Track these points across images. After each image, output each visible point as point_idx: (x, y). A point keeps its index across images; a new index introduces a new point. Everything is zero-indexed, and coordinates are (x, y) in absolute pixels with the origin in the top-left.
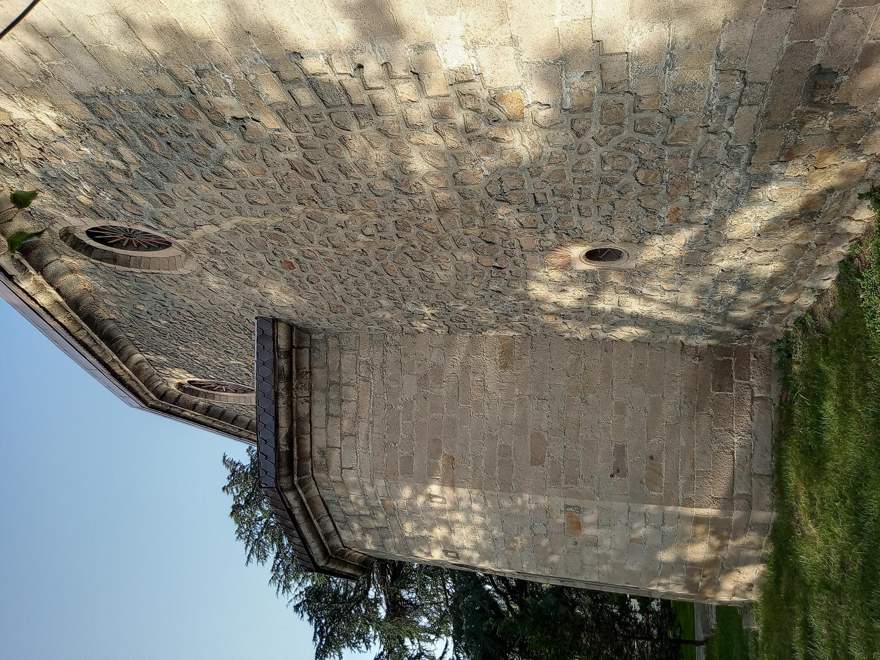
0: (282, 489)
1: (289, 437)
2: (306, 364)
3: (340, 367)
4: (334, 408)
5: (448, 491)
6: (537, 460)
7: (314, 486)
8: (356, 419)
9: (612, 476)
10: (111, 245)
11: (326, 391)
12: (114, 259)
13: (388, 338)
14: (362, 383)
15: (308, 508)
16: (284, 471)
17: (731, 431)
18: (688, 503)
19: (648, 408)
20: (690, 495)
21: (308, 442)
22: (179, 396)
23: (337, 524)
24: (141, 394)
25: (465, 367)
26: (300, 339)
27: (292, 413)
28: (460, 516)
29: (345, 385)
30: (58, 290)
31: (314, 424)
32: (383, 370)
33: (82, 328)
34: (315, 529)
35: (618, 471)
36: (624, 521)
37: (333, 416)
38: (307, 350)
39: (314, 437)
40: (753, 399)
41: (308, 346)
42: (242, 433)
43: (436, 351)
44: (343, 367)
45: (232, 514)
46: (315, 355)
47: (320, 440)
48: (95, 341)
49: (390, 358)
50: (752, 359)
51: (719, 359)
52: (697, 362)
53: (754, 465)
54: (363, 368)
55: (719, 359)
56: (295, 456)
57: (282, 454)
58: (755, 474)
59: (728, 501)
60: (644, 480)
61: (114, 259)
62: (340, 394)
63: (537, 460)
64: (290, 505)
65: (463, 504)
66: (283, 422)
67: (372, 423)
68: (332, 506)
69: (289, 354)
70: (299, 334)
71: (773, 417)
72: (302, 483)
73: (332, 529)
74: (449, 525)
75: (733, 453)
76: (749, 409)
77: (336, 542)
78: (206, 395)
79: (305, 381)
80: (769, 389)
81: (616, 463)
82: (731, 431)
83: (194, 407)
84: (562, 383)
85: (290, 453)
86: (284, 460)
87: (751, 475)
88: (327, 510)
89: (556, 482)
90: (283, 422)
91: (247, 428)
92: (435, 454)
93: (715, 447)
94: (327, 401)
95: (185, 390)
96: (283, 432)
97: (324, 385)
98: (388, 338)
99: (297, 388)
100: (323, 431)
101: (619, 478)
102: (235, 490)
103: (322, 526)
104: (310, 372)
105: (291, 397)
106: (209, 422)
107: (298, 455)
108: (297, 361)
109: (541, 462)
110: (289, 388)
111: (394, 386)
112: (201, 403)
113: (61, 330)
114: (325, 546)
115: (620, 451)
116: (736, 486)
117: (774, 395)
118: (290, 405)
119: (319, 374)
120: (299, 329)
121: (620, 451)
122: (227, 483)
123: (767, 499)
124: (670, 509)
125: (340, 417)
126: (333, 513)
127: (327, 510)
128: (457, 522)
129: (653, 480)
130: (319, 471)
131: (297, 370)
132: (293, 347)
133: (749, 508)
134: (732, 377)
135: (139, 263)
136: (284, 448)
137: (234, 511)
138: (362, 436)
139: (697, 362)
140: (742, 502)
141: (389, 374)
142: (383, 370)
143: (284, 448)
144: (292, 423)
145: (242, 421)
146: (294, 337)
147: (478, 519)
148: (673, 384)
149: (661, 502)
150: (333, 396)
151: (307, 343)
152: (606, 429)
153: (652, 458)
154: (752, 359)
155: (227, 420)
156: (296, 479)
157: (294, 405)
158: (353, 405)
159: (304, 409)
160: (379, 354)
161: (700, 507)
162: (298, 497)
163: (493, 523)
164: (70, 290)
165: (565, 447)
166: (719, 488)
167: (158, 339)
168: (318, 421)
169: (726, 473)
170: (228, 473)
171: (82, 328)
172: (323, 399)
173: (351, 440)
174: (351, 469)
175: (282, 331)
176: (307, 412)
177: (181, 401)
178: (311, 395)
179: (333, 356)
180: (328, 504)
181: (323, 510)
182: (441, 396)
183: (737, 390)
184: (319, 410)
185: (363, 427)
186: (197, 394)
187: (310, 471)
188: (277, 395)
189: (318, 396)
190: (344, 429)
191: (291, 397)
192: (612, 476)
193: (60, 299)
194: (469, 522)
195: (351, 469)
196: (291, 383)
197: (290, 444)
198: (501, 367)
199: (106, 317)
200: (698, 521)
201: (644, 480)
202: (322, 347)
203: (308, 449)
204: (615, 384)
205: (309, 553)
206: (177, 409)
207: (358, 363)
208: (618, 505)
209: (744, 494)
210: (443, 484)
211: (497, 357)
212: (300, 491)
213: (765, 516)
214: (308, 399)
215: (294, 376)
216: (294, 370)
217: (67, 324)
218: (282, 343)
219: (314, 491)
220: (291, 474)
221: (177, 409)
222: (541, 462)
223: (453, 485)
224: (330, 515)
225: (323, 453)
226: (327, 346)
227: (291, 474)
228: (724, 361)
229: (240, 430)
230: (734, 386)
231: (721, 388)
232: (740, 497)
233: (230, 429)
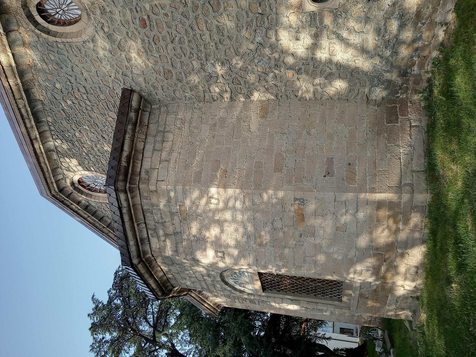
0: (118, 189)
1: (129, 158)
2: (146, 121)
3: (165, 122)
4: (158, 146)
5: (221, 190)
6: (278, 169)
7: (138, 195)
8: (171, 152)
9: (325, 176)
10: (49, 22)
11: (155, 136)
12: (48, 32)
13: (196, 105)
14: (177, 130)
15: (133, 212)
16: (121, 177)
17: (398, 146)
18: (373, 190)
19: (347, 136)
20: (374, 186)
21: (139, 165)
22: (72, 193)
23: (150, 232)
24: (48, 180)
25: (239, 119)
26: (145, 106)
27: (133, 145)
28: (228, 215)
29: (167, 132)
30: (13, 55)
31: (145, 155)
32: (190, 123)
33: (22, 98)
34: (134, 228)
35: (329, 173)
36: (332, 209)
37: (157, 150)
38: (148, 113)
39: (143, 163)
40: (411, 127)
41: (149, 111)
42: (104, 230)
43: (223, 110)
44: (167, 122)
45: (90, 329)
46: (152, 117)
47: (147, 165)
48: (28, 114)
49: (196, 116)
50: (409, 104)
51: (390, 106)
52: (376, 108)
53: (414, 165)
54: (178, 122)
55: (390, 106)
56: (130, 171)
57: (122, 167)
58: (415, 171)
59: (399, 189)
60: (345, 178)
61: (48, 32)
62: (164, 137)
63: (278, 169)
64: (121, 205)
65: (231, 204)
66: (126, 148)
67: (180, 153)
68: (148, 215)
69: (137, 111)
70: (145, 102)
71: (424, 136)
72: (131, 191)
73: (145, 236)
74: (220, 223)
75: (400, 159)
76: (409, 132)
77: (147, 248)
78: (87, 195)
79: (144, 130)
80: (421, 121)
81: (327, 168)
82: (398, 146)
83: (79, 203)
84: (296, 124)
85: (127, 168)
86: (122, 170)
87: (413, 171)
88: (145, 219)
89: (290, 182)
90: (132, 243)
91: (108, 227)
92: (216, 169)
93: (389, 155)
94: (155, 142)
95: (76, 188)
96: (125, 154)
97: (154, 133)
98: (196, 105)
99: (138, 132)
100: (149, 159)
101: (329, 178)
102: (95, 318)
103: (140, 231)
104: (148, 126)
105: (133, 136)
106: (86, 216)
107: (132, 171)
108: (141, 117)
109: (281, 170)
110: (134, 130)
111: (196, 131)
112: (83, 202)
113: (11, 95)
114: (139, 249)
115: (330, 161)
116: (403, 179)
117: (424, 124)
118: (132, 141)
119: (153, 127)
120: (146, 100)
121: (330, 161)
122: (92, 312)
123: (423, 185)
124: (362, 196)
125: (161, 150)
126: (148, 222)
127: (145, 219)
128: (226, 221)
129: (351, 178)
130: (143, 184)
131: (140, 122)
132: (140, 109)
133: (412, 192)
134: (397, 114)
135: (61, 35)
136: (124, 164)
137: (92, 327)
138: (172, 161)
139: (376, 108)
140: (407, 188)
141: (194, 125)
142: (190, 123)
143: (124, 164)
144: (132, 151)
145: (106, 221)
146: (142, 103)
147: (239, 217)
148: (362, 121)
149: (354, 190)
150: (159, 138)
151: (149, 110)
152: (321, 149)
153: (350, 164)
154: (409, 104)
155: (97, 217)
156: (128, 185)
157: (135, 142)
158: (170, 143)
159: (140, 146)
160: (189, 114)
161: (381, 192)
162: (127, 200)
163: (248, 220)
164: (21, 61)
165: (296, 161)
166: (394, 180)
167: (64, 122)
168: (147, 154)
169: (397, 171)
170: (94, 306)
171: (22, 98)
172: (153, 141)
173: (166, 163)
174: (163, 181)
175: (135, 98)
176: (142, 148)
177: (71, 196)
178: (146, 139)
179: (163, 117)
180: (145, 213)
181: (142, 217)
182: (223, 135)
183: (401, 122)
184: (149, 147)
185: (175, 155)
186: (82, 193)
187: (137, 183)
188: (125, 132)
189: (150, 139)
190: (163, 158)
191: (133, 136)
192: (325, 176)
193: (14, 65)
194: (234, 220)
195: (163, 181)
196: (135, 129)
197: (128, 162)
198: (260, 117)
199: (38, 97)
200: (380, 205)
201: (345, 178)
202: (157, 112)
203: (139, 170)
204: (327, 123)
205: (128, 249)
206: (69, 202)
207: (176, 119)
208: (329, 196)
209: (408, 183)
210: (218, 187)
211: (258, 112)
212: (129, 195)
213: (423, 197)
214: (144, 140)
215: (138, 125)
216: (138, 122)
217: (14, 88)
218: (134, 103)
219: (138, 199)
220: (125, 181)
221: (69, 202)
222: (281, 170)
223: (225, 187)
224: (145, 223)
225: (147, 172)
226: (160, 111)
227: (125, 181)
228: (392, 107)
229: (104, 227)
230: (399, 120)
231: (390, 121)
232: (406, 185)
233: (97, 225)
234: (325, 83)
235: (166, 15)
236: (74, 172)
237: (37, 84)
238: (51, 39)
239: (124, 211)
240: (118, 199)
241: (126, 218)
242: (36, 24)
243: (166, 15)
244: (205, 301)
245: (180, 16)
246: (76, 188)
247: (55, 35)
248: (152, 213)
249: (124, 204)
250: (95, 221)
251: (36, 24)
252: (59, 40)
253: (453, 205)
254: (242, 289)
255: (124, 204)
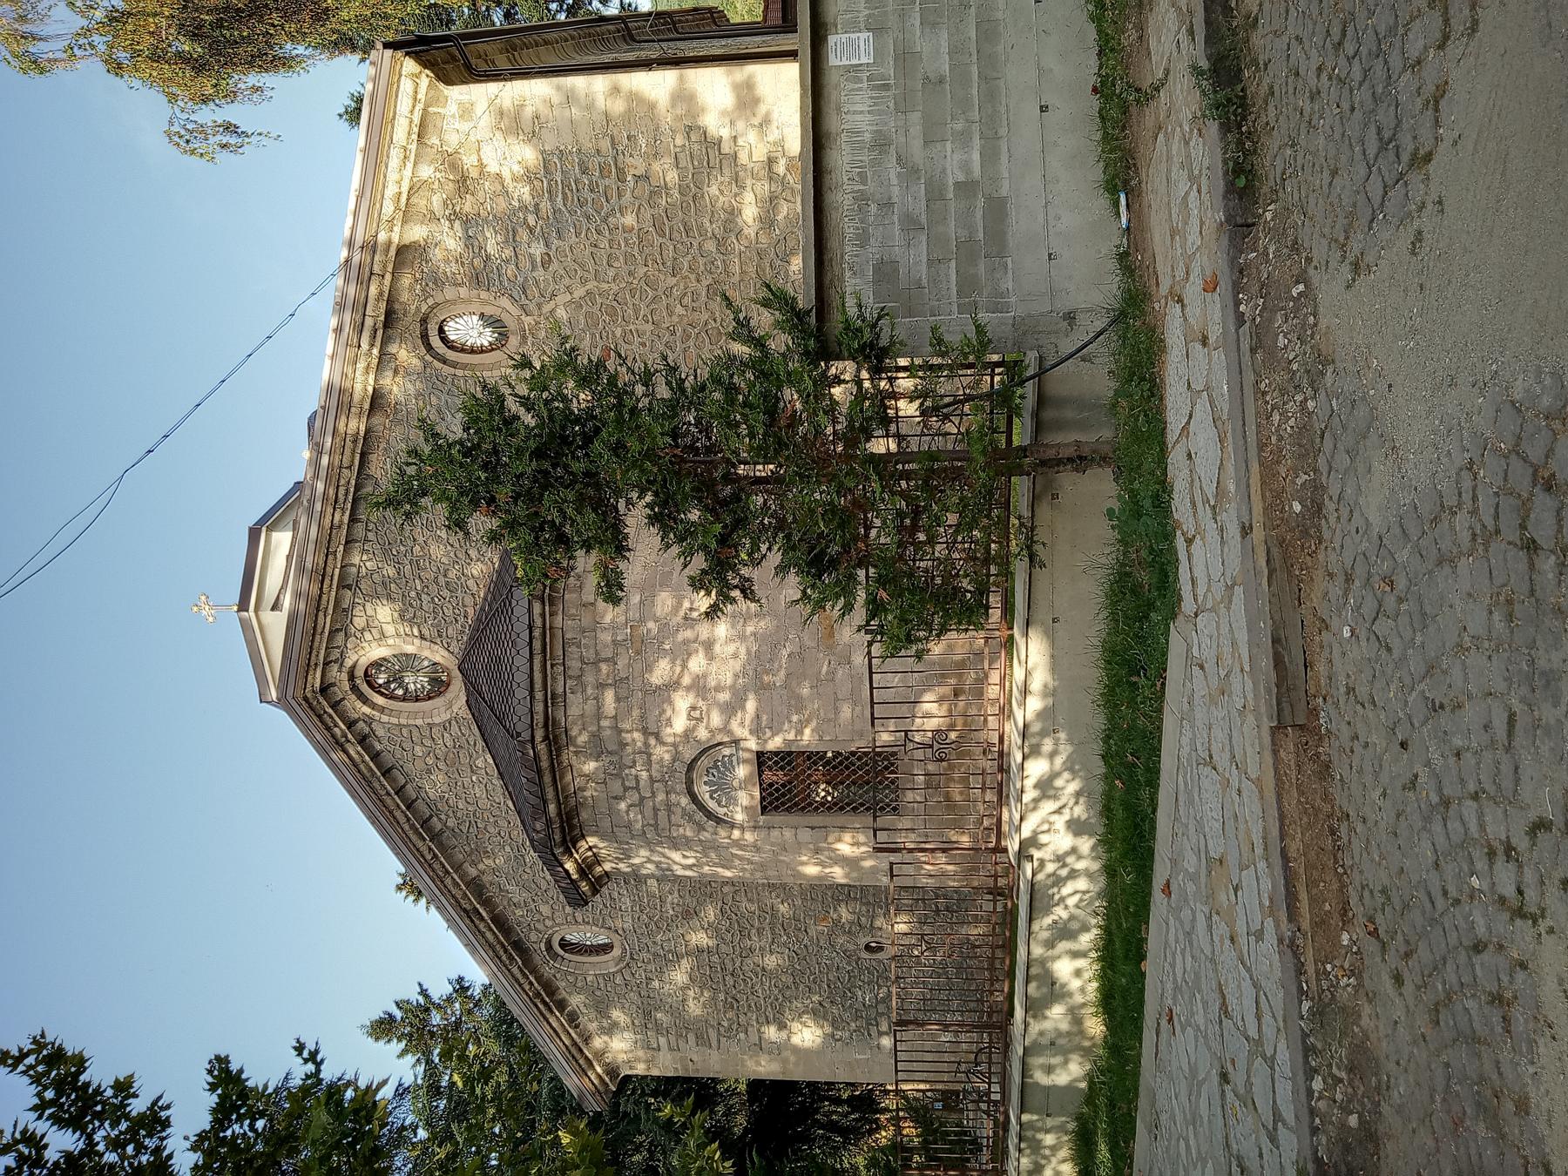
77: (560, 715)
95: (355, 689)
103: (554, 679)
162: (543, 615)
234: (1065, 865)
235: (644, 345)
236: (382, 635)
237: (382, 446)
238: (447, 370)
239: (537, 633)
240: (530, 611)
241: (537, 645)
242: (429, 348)
243: (644, 345)
244: (581, 1050)
245: (661, 348)
246: (355, 689)
247: (454, 365)
248: (579, 647)
249: (538, 622)
250: (373, 774)
251: (429, 348)
252: (459, 373)
253: (725, 133)
254: (721, 811)
255: (538, 622)
